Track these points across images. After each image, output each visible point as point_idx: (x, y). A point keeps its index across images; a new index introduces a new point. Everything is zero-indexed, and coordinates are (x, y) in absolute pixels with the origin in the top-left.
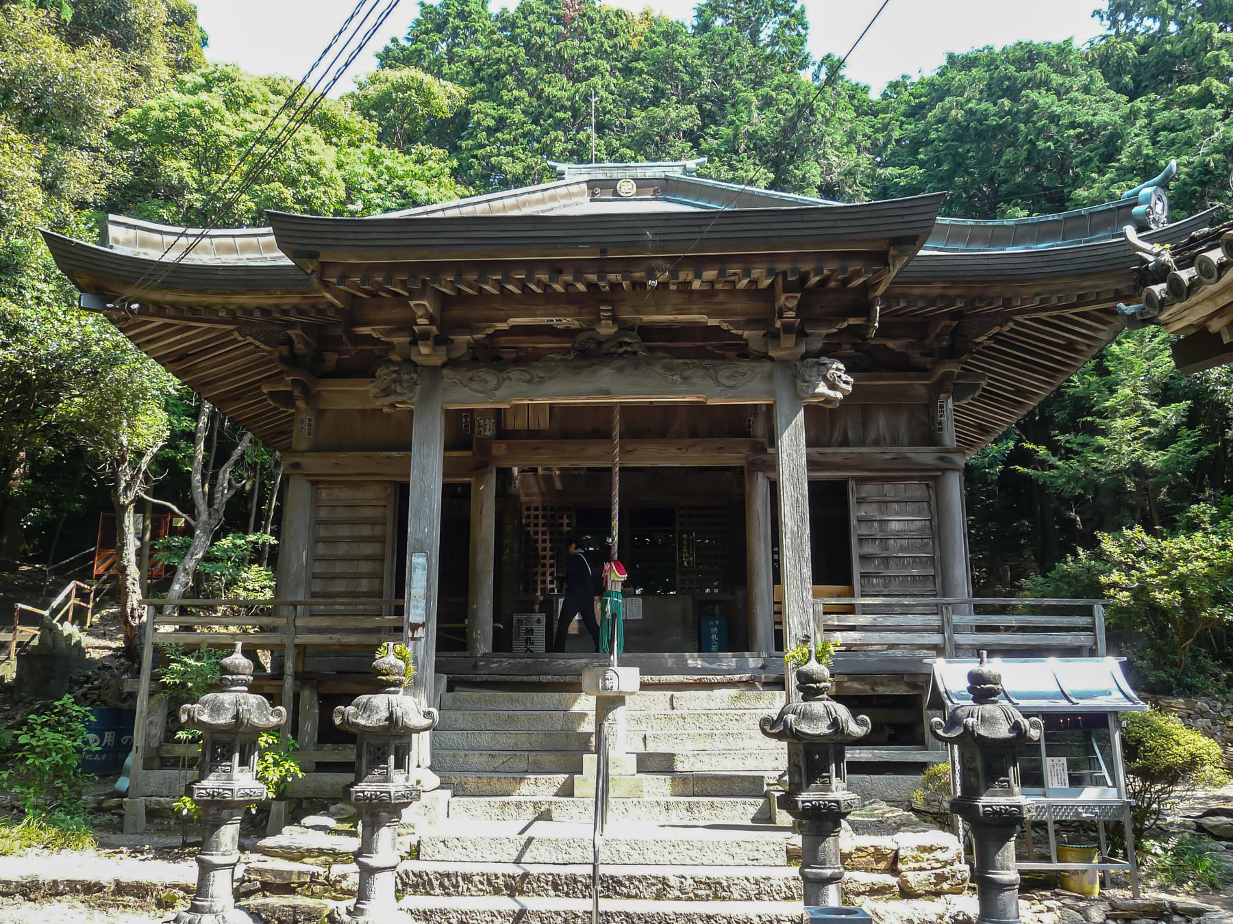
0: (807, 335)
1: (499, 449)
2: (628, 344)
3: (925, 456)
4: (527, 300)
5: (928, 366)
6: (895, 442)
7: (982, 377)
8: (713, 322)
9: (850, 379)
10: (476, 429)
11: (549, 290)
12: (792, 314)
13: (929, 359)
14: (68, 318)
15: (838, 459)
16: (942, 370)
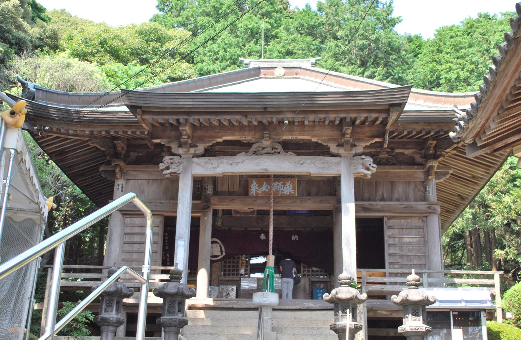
0: (356, 146)
1: (214, 200)
2: (276, 149)
3: (422, 206)
4: (231, 127)
5: (424, 163)
6: (407, 200)
7: (450, 168)
8: (314, 140)
9: (375, 166)
10: (204, 190)
11: (241, 125)
12: (348, 136)
13: (424, 160)
15: (379, 207)
16: (429, 165)
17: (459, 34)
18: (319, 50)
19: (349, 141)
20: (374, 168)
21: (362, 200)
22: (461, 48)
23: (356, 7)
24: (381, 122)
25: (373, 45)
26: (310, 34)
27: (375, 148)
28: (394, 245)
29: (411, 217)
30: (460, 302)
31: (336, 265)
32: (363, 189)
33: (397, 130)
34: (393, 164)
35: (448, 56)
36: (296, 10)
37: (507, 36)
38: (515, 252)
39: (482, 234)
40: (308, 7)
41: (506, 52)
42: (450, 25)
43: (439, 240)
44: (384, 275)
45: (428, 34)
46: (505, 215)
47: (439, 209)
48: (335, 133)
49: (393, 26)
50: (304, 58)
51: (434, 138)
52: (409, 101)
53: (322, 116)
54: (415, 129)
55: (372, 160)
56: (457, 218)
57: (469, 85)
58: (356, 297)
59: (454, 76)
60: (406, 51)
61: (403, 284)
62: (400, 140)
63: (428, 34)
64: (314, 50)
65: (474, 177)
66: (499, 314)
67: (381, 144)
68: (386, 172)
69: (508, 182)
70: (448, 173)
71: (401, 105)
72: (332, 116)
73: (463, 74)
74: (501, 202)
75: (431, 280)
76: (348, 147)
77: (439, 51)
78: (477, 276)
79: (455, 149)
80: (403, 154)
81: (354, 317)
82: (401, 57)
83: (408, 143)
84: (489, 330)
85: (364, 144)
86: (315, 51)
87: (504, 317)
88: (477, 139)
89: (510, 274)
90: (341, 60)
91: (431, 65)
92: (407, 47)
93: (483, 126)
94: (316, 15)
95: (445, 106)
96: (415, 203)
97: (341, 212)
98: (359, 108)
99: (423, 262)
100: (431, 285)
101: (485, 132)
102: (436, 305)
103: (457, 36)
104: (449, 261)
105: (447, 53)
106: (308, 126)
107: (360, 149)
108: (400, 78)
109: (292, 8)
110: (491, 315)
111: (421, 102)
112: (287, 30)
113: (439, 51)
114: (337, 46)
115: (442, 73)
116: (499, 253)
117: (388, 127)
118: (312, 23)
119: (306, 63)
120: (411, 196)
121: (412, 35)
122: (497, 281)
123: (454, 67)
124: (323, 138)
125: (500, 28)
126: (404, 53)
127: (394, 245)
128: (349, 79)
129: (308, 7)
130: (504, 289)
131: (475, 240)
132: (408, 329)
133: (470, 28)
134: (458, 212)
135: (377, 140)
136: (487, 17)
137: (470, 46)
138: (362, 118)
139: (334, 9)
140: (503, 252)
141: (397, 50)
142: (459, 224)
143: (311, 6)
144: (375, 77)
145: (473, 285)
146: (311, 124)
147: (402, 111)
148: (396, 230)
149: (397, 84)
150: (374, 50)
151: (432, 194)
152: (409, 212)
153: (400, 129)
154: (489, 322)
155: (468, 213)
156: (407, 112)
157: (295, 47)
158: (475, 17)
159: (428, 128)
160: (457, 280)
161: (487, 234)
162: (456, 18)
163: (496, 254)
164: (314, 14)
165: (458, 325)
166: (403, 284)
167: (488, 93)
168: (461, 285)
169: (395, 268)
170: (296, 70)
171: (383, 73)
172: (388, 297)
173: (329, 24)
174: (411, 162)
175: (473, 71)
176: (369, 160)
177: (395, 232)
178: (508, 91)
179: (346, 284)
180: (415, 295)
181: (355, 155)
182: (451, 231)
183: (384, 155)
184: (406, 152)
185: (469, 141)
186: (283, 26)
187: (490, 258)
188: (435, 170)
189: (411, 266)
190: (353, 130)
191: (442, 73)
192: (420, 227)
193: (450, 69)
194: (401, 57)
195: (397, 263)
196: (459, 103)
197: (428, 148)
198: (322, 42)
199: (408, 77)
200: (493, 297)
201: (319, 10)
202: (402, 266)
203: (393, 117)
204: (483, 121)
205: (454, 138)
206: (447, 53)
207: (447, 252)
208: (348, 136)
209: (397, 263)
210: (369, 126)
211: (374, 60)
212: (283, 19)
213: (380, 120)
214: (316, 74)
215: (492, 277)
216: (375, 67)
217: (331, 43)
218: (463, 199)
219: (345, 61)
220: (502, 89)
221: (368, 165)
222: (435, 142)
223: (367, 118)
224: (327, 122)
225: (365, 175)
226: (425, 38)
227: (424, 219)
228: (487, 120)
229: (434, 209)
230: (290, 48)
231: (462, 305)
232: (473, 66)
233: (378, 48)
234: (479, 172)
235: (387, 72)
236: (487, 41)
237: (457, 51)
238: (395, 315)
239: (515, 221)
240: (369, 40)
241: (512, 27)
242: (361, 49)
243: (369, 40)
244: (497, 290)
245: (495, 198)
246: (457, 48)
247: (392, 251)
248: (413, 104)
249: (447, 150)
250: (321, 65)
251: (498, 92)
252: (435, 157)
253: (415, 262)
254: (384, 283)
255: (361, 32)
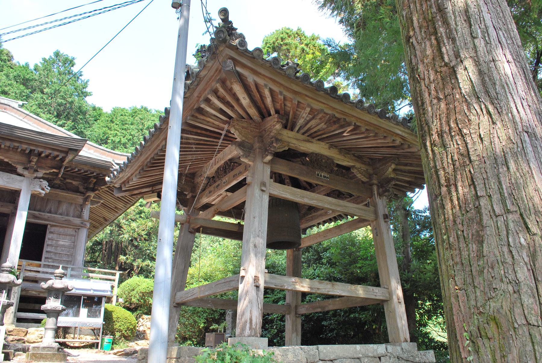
3: (77, 221)
6: (68, 215)
7: (102, 199)
8: (6, 160)
9: (49, 188)
12: (34, 163)
14: (191, 321)
15: (46, 217)
17: (127, 114)
18: (28, 97)
19: (33, 167)
20: (48, 190)
21: (35, 210)
22: (126, 124)
23: (63, 76)
24: (61, 159)
25: (68, 105)
26: (24, 84)
27: (52, 175)
28: (52, 246)
29: (68, 227)
30: (90, 290)
31: (4, 254)
32: (36, 202)
33: (71, 166)
34: (63, 189)
35: (117, 126)
36: (17, 64)
37: (155, 125)
38: (132, 258)
39: (114, 244)
40: (27, 65)
41: (153, 135)
42: (122, 107)
43: (84, 243)
44: (40, 266)
45: (107, 109)
46: (131, 234)
47: (88, 225)
48: (24, 159)
49: (85, 97)
50: (15, 99)
51: (95, 177)
52: (84, 149)
53: (17, 144)
54: (83, 169)
55: (47, 184)
56: (100, 232)
57: (125, 148)
58: (13, 281)
59: (118, 140)
60: (90, 115)
61: (52, 273)
62: (71, 173)
63: (107, 109)
64: (24, 96)
65: (116, 208)
66: (114, 299)
67: (57, 174)
68: (56, 194)
69: (137, 214)
70: (100, 202)
71: (77, 151)
72: (24, 146)
73: (124, 140)
74: (130, 226)
75: (74, 273)
76: (32, 171)
77: (112, 122)
78: (105, 273)
79: (107, 187)
80: (71, 183)
81: (9, 297)
82: (85, 119)
83: (76, 177)
84: (106, 309)
85: (44, 172)
86: (25, 97)
87: (117, 301)
88: (123, 185)
89: (127, 272)
90: (42, 108)
91: (104, 129)
92: (91, 112)
93: (129, 178)
94: (32, 72)
95: (108, 158)
96: (73, 218)
97: (16, 216)
98: (46, 145)
99: (70, 259)
100: (72, 276)
101: (128, 182)
102: (73, 291)
103: (125, 115)
104: (89, 258)
105: (117, 125)
106: (4, 149)
107: (40, 174)
108: (82, 132)
109: (14, 62)
110: (109, 300)
111: (92, 151)
112: (7, 76)
113: (112, 122)
114: (42, 98)
115: (110, 136)
116: (122, 258)
117: (65, 163)
118: (27, 77)
119: (15, 104)
120: (71, 213)
121: (97, 106)
122: (117, 278)
123: (119, 134)
124: (13, 160)
125: (152, 118)
126: (88, 116)
127: (52, 246)
128: (45, 123)
129: (27, 65)
130: (121, 281)
131: (109, 247)
132: (49, 308)
133: (135, 113)
134: (101, 228)
135: (55, 170)
136: (146, 109)
137: (132, 124)
138: (47, 153)
139: (46, 72)
140: (125, 258)
141: (84, 113)
142: (100, 236)
143: (30, 66)
144: (64, 126)
145: (100, 279)
146: (6, 148)
147: (77, 155)
148: (55, 235)
149: (79, 135)
150: (68, 109)
151: (86, 214)
152: (68, 224)
153: (74, 166)
154: (106, 305)
155: (108, 229)
156: (80, 156)
157: (10, 89)
158: (139, 107)
159: (93, 170)
160: (91, 275)
161: (117, 244)
162: (128, 103)
163: (120, 258)
164: (30, 71)
165: (86, 305)
166: (52, 273)
167: (136, 158)
168: (92, 278)
169: (49, 262)
170: (5, 106)
171: (71, 125)
172: (40, 281)
173: (40, 82)
174: (76, 190)
175: (130, 140)
176: (45, 183)
177: (55, 236)
178: (148, 160)
179: (7, 271)
180: (58, 284)
181: (36, 178)
182: (94, 239)
183: (57, 182)
184: (74, 183)
185: (117, 186)
186: (4, 72)
187: (116, 260)
188: (92, 198)
189: (60, 262)
190: (37, 160)
191: (110, 136)
192: (72, 235)
193: (116, 135)
194: (85, 119)
195: (51, 258)
196: (116, 158)
197: (90, 183)
198: (32, 93)
199: (88, 133)
200: (112, 287)
201: (35, 70)
202: (54, 260)
203: (70, 157)
204: (129, 175)
205: (108, 182)
206: (117, 125)
207: (89, 253)
208: (34, 163)
209: (51, 258)
210: (51, 159)
211: (67, 115)
212: (5, 67)
213: (60, 157)
214: (21, 113)
215: (114, 274)
216: (66, 120)
217: (39, 95)
218: (106, 220)
219: (46, 110)
220: (145, 158)
221: (44, 187)
222: (95, 180)
223: (50, 154)
224: (19, 150)
225: (40, 193)
226: (104, 111)
227: (77, 230)
228: (132, 175)
229: (85, 225)
230: (6, 89)
231: (91, 293)
232: (131, 137)
233: (71, 108)
234: (120, 205)
235: (73, 126)
236: (143, 124)
237: (123, 125)
238: (42, 295)
239: (136, 239)
240: (66, 101)
241: (160, 120)
242: (60, 105)
243: (66, 101)
244: (116, 284)
245: (127, 223)
246: (124, 123)
247: (49, 249)
248: (86, 152)
249: (102, 187)
250: (26, 108)
251: (142, 159)
252: (93, 190)
253: (64, 259)
254: (38, 272)
255: (62, 94)
